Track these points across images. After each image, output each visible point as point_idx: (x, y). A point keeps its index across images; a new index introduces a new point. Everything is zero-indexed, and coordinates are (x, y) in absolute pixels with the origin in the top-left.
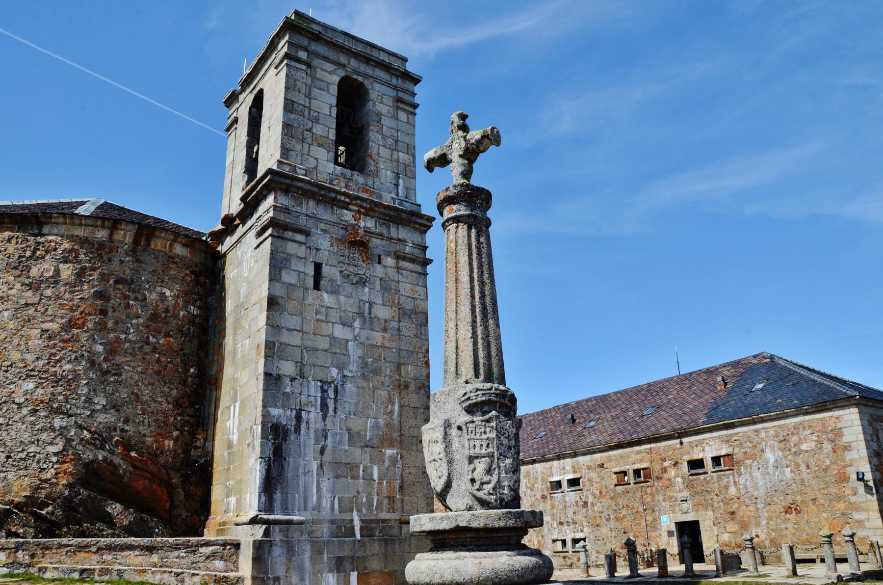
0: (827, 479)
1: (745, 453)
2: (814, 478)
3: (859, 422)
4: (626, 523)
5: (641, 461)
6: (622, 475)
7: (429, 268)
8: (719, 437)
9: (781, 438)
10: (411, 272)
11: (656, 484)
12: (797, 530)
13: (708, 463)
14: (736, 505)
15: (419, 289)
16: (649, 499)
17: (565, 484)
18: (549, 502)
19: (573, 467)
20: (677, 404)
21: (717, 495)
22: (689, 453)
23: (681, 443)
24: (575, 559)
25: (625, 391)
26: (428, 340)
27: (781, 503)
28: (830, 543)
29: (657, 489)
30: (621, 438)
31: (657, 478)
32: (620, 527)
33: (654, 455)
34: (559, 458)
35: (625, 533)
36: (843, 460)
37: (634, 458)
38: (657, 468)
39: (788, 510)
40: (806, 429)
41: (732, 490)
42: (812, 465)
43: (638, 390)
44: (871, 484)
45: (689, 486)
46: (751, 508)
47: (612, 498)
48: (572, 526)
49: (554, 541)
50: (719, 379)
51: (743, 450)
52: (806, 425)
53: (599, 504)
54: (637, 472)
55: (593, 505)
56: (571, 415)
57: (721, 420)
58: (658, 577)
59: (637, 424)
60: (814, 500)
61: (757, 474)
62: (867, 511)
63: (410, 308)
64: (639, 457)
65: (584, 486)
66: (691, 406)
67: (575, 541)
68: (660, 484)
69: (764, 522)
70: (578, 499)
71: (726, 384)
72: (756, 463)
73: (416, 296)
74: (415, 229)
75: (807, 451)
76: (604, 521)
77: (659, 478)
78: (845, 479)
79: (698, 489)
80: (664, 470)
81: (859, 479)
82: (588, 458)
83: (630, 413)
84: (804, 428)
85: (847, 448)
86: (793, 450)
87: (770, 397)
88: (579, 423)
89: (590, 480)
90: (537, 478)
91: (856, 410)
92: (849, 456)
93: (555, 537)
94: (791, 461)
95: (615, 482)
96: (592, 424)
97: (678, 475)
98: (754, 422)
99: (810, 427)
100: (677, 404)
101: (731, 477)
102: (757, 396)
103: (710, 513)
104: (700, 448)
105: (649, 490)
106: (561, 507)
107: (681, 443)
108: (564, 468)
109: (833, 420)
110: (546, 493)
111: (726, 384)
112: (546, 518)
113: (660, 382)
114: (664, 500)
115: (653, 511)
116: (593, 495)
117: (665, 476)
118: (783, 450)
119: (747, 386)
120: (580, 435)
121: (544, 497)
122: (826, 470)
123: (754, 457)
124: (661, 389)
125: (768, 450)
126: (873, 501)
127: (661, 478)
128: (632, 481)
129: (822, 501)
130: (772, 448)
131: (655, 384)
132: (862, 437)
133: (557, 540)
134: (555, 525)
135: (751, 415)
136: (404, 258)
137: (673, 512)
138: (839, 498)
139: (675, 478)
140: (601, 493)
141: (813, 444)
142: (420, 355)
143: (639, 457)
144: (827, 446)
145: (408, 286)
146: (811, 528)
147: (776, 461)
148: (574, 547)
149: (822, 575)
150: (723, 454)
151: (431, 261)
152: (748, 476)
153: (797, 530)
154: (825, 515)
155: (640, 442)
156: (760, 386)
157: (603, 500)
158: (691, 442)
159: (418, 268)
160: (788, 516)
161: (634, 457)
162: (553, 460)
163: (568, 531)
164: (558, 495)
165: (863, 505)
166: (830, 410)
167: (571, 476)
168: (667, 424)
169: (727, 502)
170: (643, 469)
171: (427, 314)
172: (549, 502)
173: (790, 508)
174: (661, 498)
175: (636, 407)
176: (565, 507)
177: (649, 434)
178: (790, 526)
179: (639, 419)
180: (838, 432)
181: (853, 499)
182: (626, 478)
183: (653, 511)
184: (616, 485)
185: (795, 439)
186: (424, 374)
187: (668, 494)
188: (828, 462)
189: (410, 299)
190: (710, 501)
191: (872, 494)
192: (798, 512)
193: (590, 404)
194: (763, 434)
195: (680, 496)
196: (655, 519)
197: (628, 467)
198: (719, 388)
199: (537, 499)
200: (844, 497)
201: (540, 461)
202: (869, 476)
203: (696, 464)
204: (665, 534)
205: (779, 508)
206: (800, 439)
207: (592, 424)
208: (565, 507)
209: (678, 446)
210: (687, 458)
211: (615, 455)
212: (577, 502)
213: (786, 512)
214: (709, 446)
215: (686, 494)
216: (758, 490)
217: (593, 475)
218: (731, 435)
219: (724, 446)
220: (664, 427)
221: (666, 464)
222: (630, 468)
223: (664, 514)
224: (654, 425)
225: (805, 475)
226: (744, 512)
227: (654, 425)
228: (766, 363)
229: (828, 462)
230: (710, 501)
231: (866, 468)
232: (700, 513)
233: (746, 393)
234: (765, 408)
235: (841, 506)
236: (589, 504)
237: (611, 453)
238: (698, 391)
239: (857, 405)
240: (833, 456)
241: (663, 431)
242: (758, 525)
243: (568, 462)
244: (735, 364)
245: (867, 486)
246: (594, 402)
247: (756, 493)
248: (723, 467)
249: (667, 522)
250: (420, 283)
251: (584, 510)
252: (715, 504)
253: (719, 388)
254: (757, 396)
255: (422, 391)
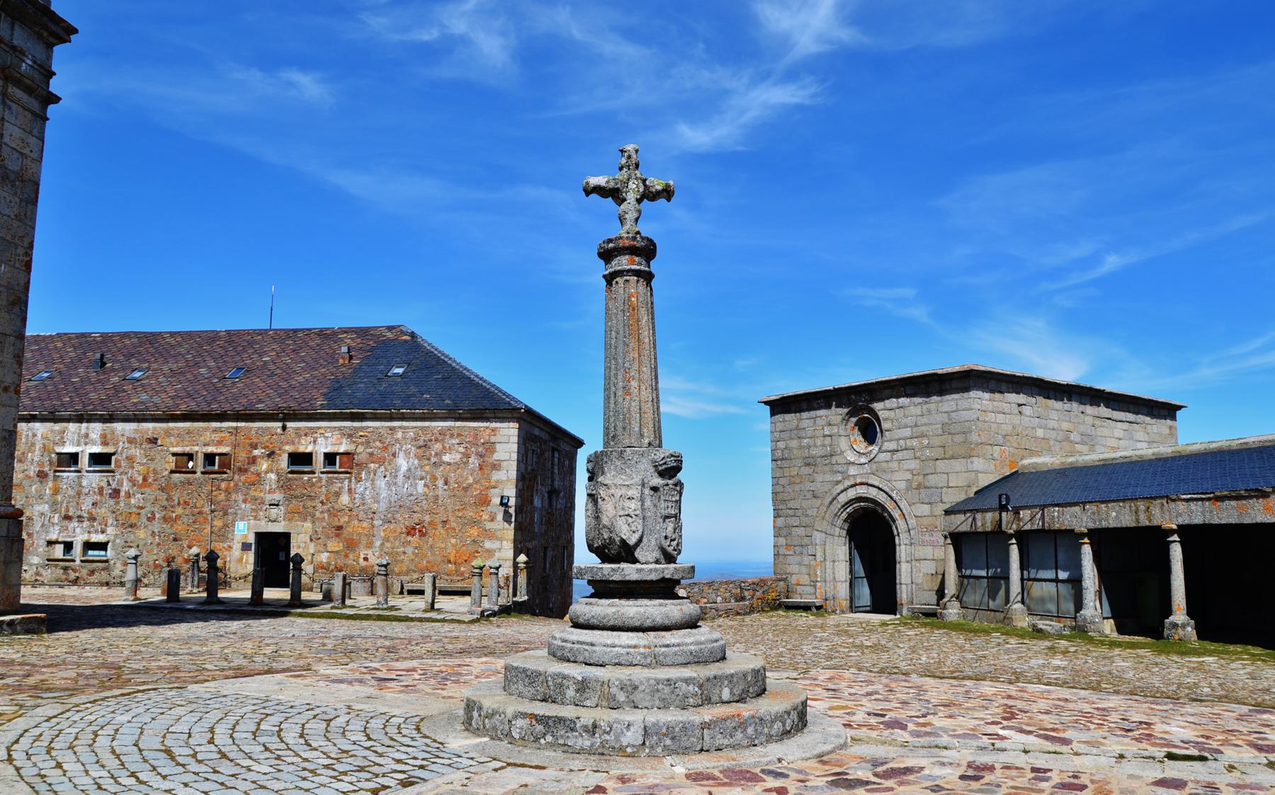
0: (466, 500)
1: (371, 454)
2: (450, 497)
3: (515, 439)
4: (179, 527)
5: (220, 443)
6: (186, 458)
7: (52, 109)
8: (340, 429)
9: (421, 443)
10: (24, 109)
11: (236, 477)
12: (416, 555)
13: (319, 461)
14: (346, 519)
15: (33, 141)
16: (222, 497)
17: (84, 461)
18: (50, 484)
19: (104, 436)
20: (278, 371)
21: (322, 502)
22: (293, 443)
23: (284, 428)
24: (84, 572)
25: (190, 335)
26: (34, 228)
27: (404, 520)
28: (480, 575)
29: (236, 485)
30: (193, 406)
31: (240, 470)
32: (170, 531)
33: (241, 438)
34: (80, 419)
35: (175, 540)
36: (489, 480)
37: (209, 438)
38: (242, 456)
39: (410, 531)
40: (453, 439)
41: (345, 499)
42: (452, 481)
43: (213, 337)
44: (512, 511)
45: (284, 486)
46: (365, 525)
47: (162, 489)
48: (86, 524)
49: (50, 543)
50: (344, 349)
51: (369, 450)
52: (455, 432)
53: (139, 496)
54: (209, 458)
55: (128, 495)
56: (101, 352)
57: (344, 407)
58: (249, 604)
59: (218, 389)
60: (444, 522)
61: (381, 483)
62: (501, 540)
63: (17, 169)
64: (216, 437)
65: (118, 465)
66: (300, 379)
67: (88, 546)
68: (243, 478)
69: (378, 543)
70: (104, 484)
71: (351, 358)
72: (382, 469)
73: (26, 151)
74: (39, 36)
75: (449, 464)
76: (144, 520)
77: (242, 470)
78: (485, 501)
79: (297, 493)
80: (253, 460)
81: (502, 504)
82: (133, 426)
83: (202, 371)
84: (452, 436)
85: (496, 466)
86: (433, 460)
87: (413, 389)
88: (113, 370)
89: (130, 459)
90: (33, 444)
91: (517, 425)
92: (496, 476)
93: (53, 537)
94: (427, 473)
95: (173, 466)
96: (137, 375)
97: (271, 472)
98: (391, 418)
99: (459, 435)
100: (278, 371)
101: (346, 482)
102: (396, 384)
103: (308, 525)
104: (309, 439)
105: (223, 485)
106: (71, 492)
107: (284, 428)
108: (87, 436)
109: (488, 431)
110: (46, 469)
111: (351, 358)
112: (672, 565)
113: (247, 332)
114: (245, 501)
115: (226, 514)
116: (132, 481)
117: (253, 469)
118: (420, 458)
119: (381, 368)
120: (117, 389)
121: (42, 475)
122: (466, 489)
123: (381, 461)
124: (251, 344)
125: (402, 455)
126: (509, 531)
127: (246, 471)
128: (200, 469)
129: (453, 524)
130: (407, 453)
131: (239, 333)
132: (515, 456)
133: (57, 542)
134: (56, 519)
135: (389, 407)
136: (18, 83)
137: (256, 518)
138: (475, 523)
139: (267, 472)
140: (145, 479)
141: (458, 456)
142: (20, 251)
143: (216, 437)
144: (474, 461)
145: (17, 132)
146: (433, 555)
147: (409, 470)
148: (84, 554)
149: (465, 610)
150: (341, 450)
151: (56, 99)
152: (368, 484)
153: (416, 555)
154: (453, 541)
155: (222, 417)
156: (400, 371)
157: (147, 490)
158: (298, 429)
159: (35, 105)
160: (409, 538)
161: (208, 436)
162: (68, 420)
163: (78, 530)
164: (68, 476)
165: (499, 534)
166: (487, 419)
167: (97, 449)
168: (264, 396)
169: (333, 513)
170: (220, 454)
171: (38, 185)
172: (50, 484)
173: (414, 529)
174: (241, 497)
175: (212, 364)
176: (79, 494)
177: (238, 407)
178: (409, 550)
179: (224, 380)
180: (490, 447)
181: (489, 525)
182: (191, 464)
183: (226, 514)
184: (172, 472)
185: (438, 446)
186: (22, 282)
187: (252, 493)
188: (471, 480)
189: (16, 155)
190: (311, 510)
191: (509, 522)
192: (423, 535)
193: (127, 342)
194: (399, 435)
195: (268, 498)
196: (226, 526)
197: (196, 448)
198: (341, 361)
199: (28, 477)
200: (480, 522)
201: (43, 419)
202: (512, 502)
203: (301, 460)
204: (237, 547)
205: (401, 528)
206: (444, 448)
207: (137, 375)
208: (79, 494)
209: (279, 431)
210: (289, 448)
211: (178, 429)
212: (101, 490)
213: (408, 534)
214: (324, 439)
215: (278, 496)
216: (378, 502)
217: (136, 452)
218: (355, 428)
219: (344, 441)
220: (260, 401)
221: (256, 452)
222: (200, 450)
223: (242, 519)
224: (245, 396)
225: (440, 492)
226: (355, 528)
227: (245, 396)
228: (406, 341)
229: (471, 480)
230: (311, 510)
231: (511, 492)
232: (294, 523)
233: (380, 376)
234: (406, 400)
235: (474, 532)
236: (122, 494)
237: (172, 425)
238: (308, 359)
239: (518, 420)
240: (477, 474)
241: (260, 406)
242: (370, 545)
243: (96, 429)
244: (363, 332)
245: (506, 512)
246: (135, 340)
247: (375, 506)
248: (337, 468)
249: (244, 530)
250: (35, 132)
251: (112, 502)
252: (318, 514)
253: (341, 361)
254: (396, 384)
255: (16, 310)
